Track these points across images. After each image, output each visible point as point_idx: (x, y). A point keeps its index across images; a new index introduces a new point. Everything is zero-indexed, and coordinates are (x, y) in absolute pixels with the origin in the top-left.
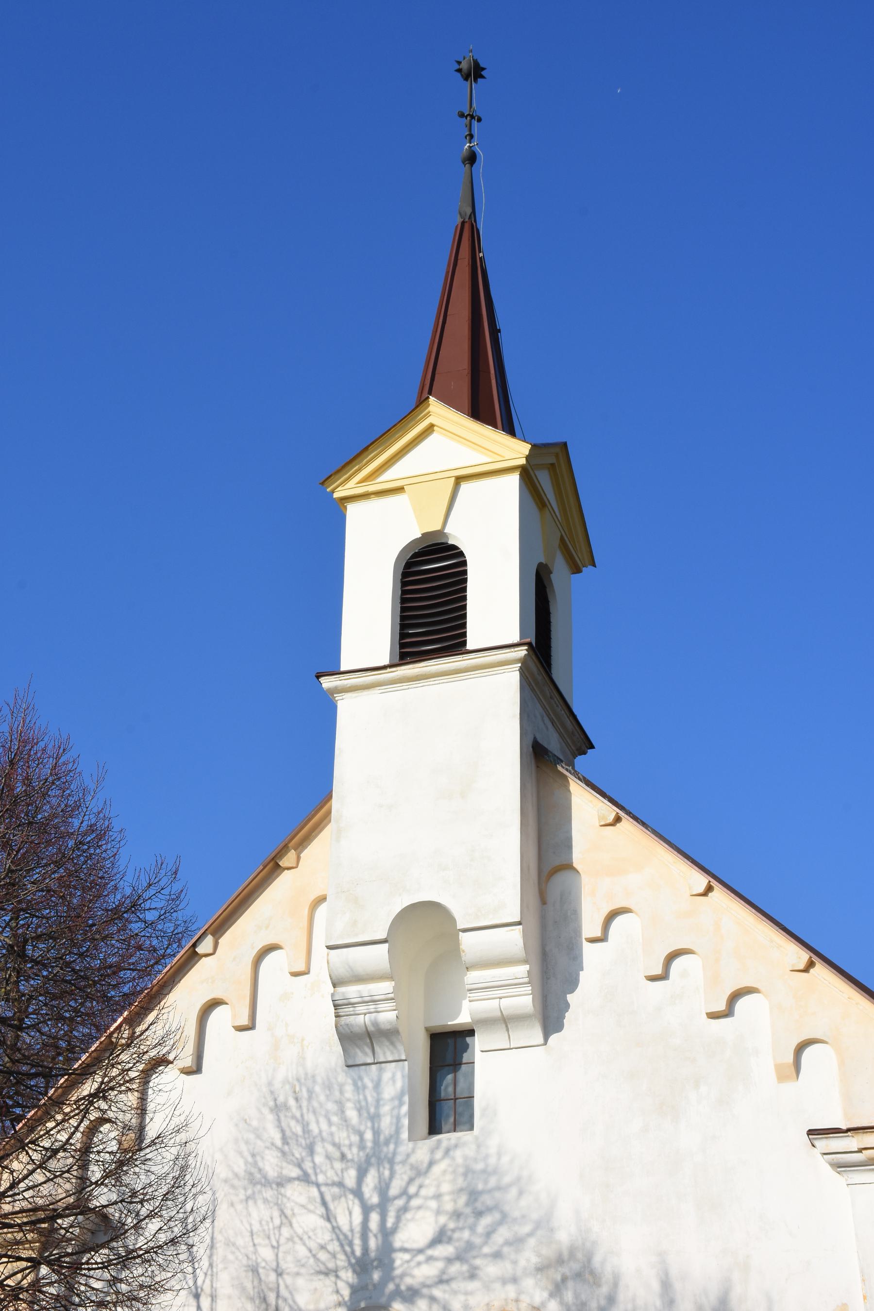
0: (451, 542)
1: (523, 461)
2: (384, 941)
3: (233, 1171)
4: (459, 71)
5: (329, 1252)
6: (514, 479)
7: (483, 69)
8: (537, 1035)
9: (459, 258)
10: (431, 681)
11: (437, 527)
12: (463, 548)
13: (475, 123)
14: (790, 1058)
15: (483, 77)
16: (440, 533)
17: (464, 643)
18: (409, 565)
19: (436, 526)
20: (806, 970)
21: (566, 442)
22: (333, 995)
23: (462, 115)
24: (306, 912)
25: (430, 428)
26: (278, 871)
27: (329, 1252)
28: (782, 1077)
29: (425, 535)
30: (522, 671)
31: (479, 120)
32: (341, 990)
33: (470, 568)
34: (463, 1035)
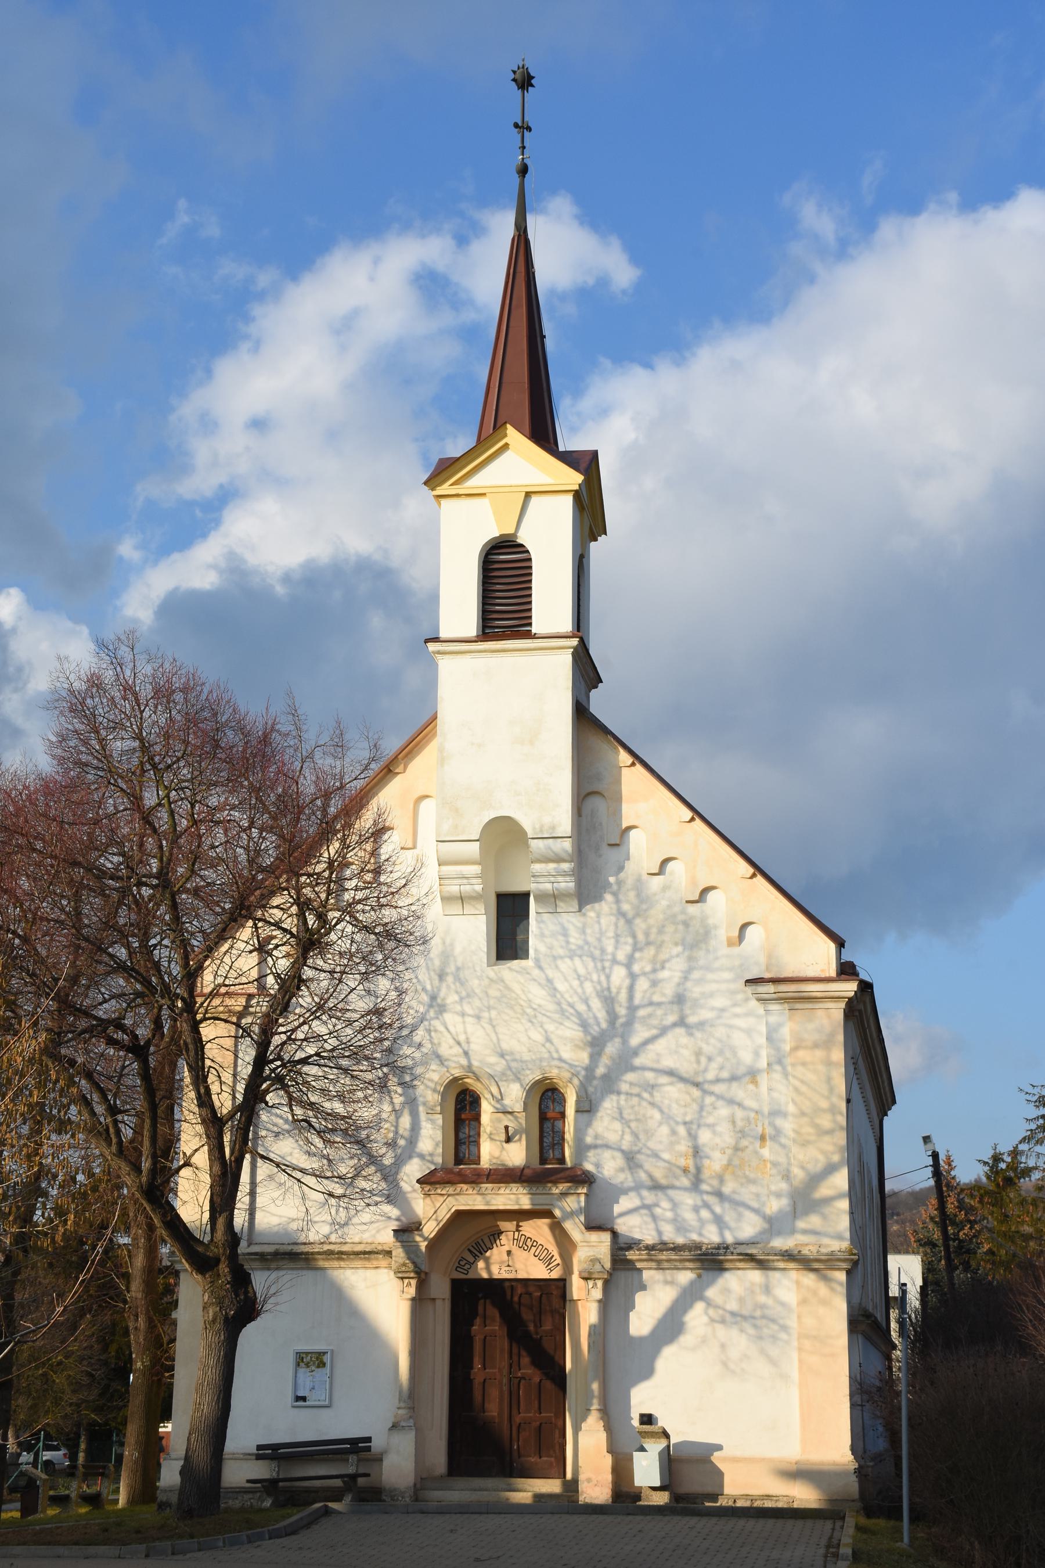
0: (520, 541)
1: (576, 487)
2: (478, 840)
4: (514, 80)
5: (657, 1225)
6: (569, 499)
7: (533, 77)
10: (508, 654)
11: (512, 531)
13: (526, 133)
15: (532, 86)
17: (527, 621)
20: (751, 878)
21: (596, 452)
23: (516, 125)
24: (411, 806)
25: (506, 446)
26: (391, 774)
27: (657, 1225)
30: (573, 654)
31: (927, 1139)
32: (444, 868)
33: (534, 564)
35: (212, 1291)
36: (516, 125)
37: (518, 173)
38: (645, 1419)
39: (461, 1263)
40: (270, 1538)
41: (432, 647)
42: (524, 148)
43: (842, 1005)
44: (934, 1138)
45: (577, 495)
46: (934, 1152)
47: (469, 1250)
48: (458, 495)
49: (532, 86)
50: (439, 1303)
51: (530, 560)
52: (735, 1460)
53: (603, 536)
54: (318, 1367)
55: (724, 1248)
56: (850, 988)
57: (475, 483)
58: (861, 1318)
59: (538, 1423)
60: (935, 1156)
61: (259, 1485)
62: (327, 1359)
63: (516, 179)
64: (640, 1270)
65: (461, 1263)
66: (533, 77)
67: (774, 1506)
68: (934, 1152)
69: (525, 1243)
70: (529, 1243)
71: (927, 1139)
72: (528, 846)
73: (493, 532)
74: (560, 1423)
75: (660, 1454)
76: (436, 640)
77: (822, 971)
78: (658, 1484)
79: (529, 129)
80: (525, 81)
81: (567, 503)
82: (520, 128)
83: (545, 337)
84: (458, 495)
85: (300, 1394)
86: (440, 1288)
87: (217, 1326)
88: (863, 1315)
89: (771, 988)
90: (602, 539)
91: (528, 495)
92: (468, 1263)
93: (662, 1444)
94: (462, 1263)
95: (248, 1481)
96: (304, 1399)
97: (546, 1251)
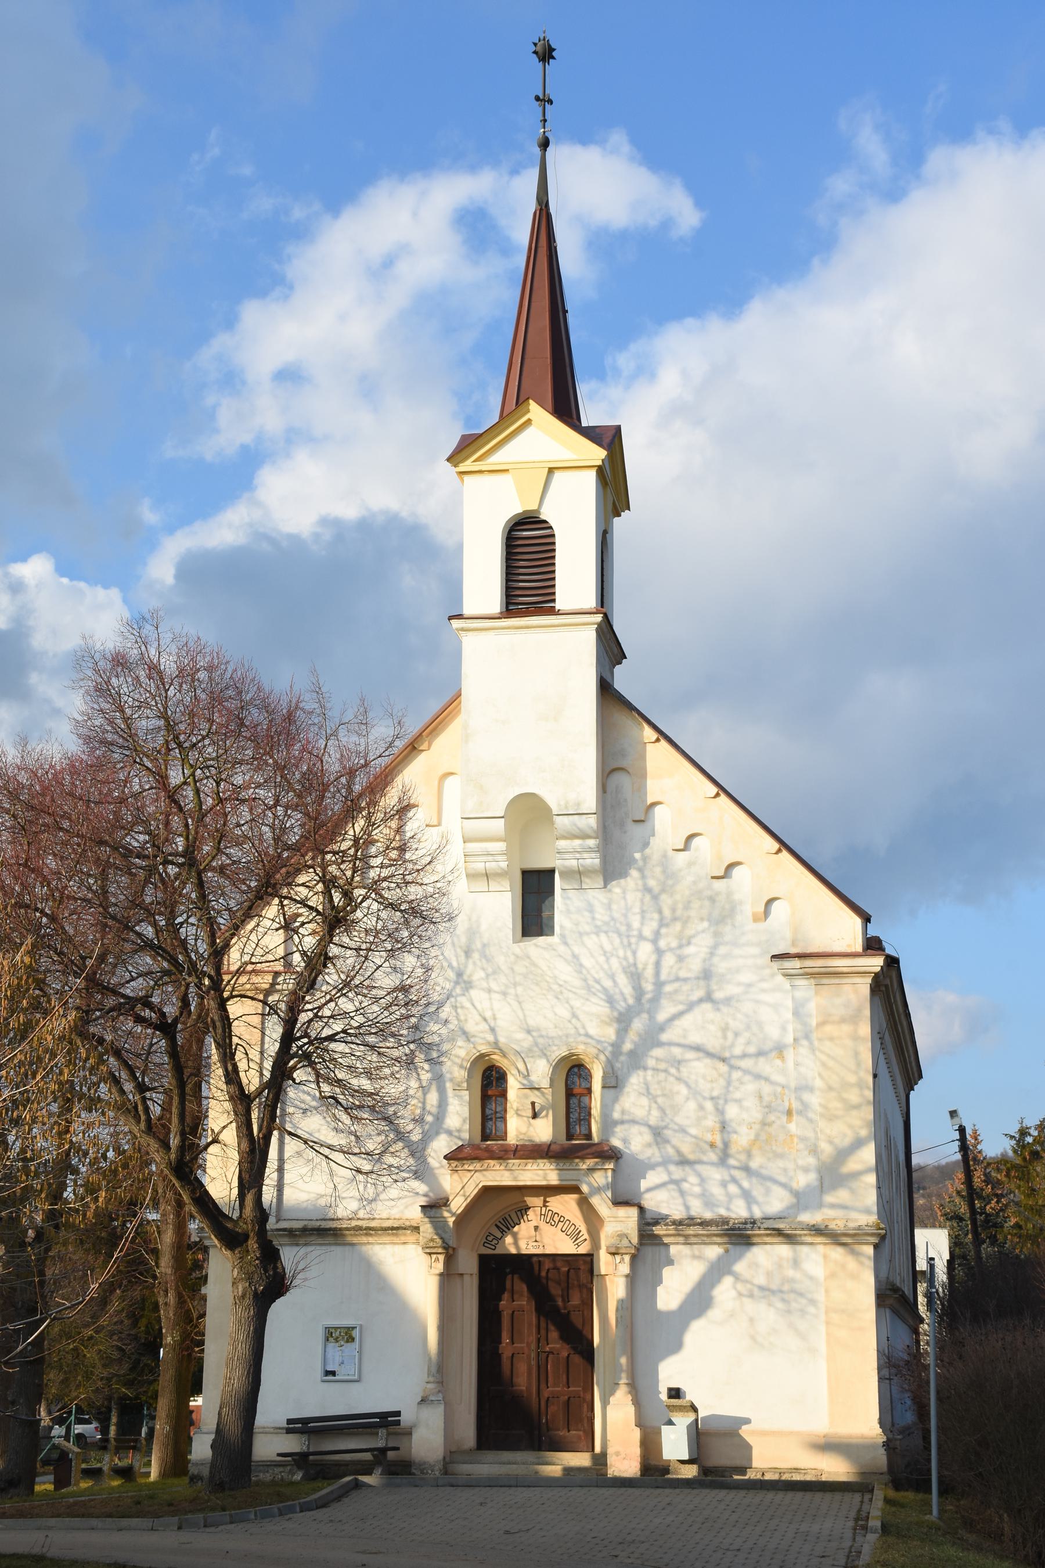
0: (543, 517)
1: (600, 463)
2: (502, 817)
3: (490, 1026)
4: (535, 52)
6: (592, 474)
7: (554, 50)
8: (600, 883)
9: (913, 1151)
11: (535, 507)
12: (552, 523)
14: (762, 909)
15: (553, 58)
16: (538, 511)
17: (551, 597)
18: (511, 530)
19: (533, 506)
22: (464, 849)
24: (436, 783)
28: (756, 919)
29: (525, 512)
30: (597, 630)
32: (468, 845)
33: (558, 540)
34: (548, 874)
35: (241, 1267)
36: (537, 99)
37: (540, 146)
38: (673, 1393)
39: (489, 1238)
40: (301, 1511)
41: (456, 624)
42: (545, 121)
43: (869, 980)
44: (960, 1113)
45: (600, 471)
46: (961, 1126)
47: (496, 1225)
48: (480, 472)
49: (553, 58)
50: (467, 1278)
51: (553, 536)
52: (764, 1433)
53: (627, 511)
54: (347, 1342)
55: (751, 1223)
56: (876, 963)
57: (499, 458)
58: (888, 1292)
59: (566, 1397)
60: (962, 1130)
61: (289, 1459)
62: (356, 1334)
63: (537, 151)
64: (667, 1245)
65: (489, 1238)
66: (554, 50)
67: (802, 1479)
68: (961, 1126)
69: (552, 1218)
70: (556, 1219)
71: (953, 1114)
72: (552, 823)
73: (516, 508)
74: (588, 1397)
75: (689, 1427)
76: (459, 617)
77: (849, 946)
78: (686, 1457)
79: (550, 102)
80: (546, 54)
81: (590, 477)
82: (541, 101)
83: (567, 311)
84: (480, 472)
85: (329, 1369)
86: (468, 1264)
87: (247, 1301)
88: (890, 1289)
89: (797, 963)
90: (625, 514)
91: (551, 471)
92: (496, 1238)
93: (690, 1418)
94: (490, 1238)
95: (279, 1455)
96: (333, 1373)
97: (573, 1226)
